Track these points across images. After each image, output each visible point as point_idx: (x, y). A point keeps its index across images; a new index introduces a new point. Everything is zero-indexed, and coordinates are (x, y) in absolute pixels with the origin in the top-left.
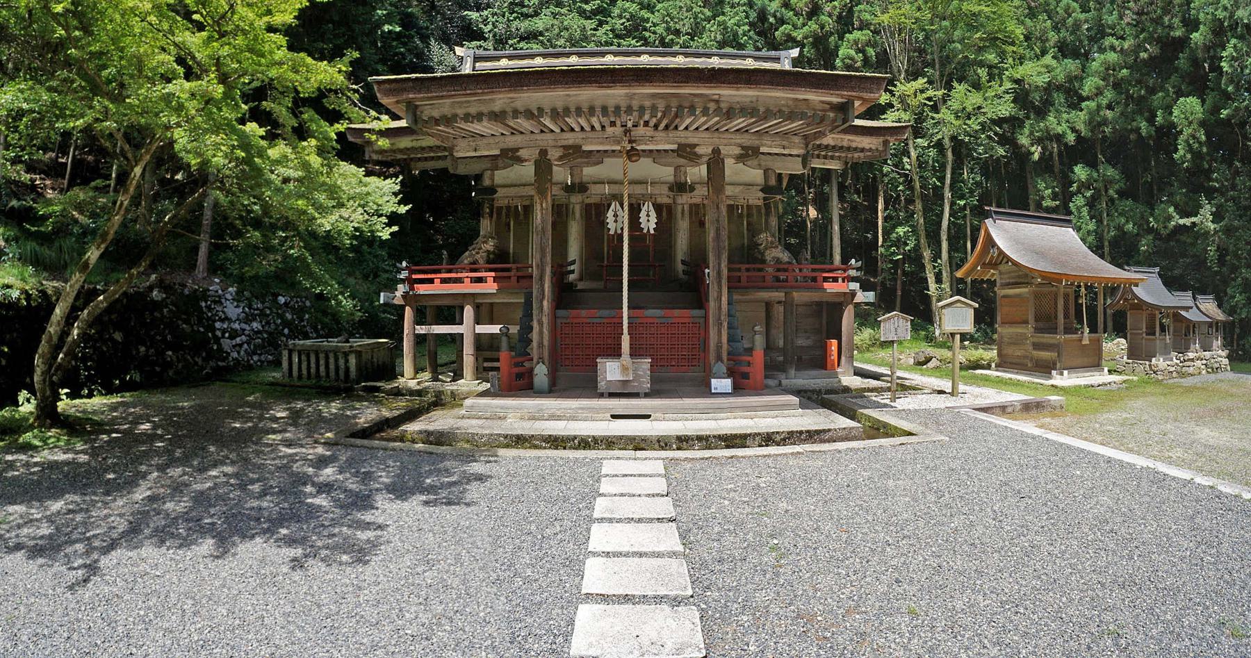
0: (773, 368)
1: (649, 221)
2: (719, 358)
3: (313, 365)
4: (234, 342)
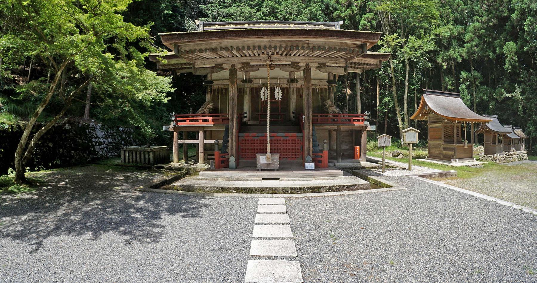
0: (332, 158)
1: (279, 95)
2: (309, 154)
3: (134, 157)
4: (100, 147)
